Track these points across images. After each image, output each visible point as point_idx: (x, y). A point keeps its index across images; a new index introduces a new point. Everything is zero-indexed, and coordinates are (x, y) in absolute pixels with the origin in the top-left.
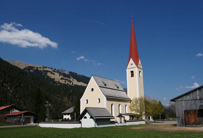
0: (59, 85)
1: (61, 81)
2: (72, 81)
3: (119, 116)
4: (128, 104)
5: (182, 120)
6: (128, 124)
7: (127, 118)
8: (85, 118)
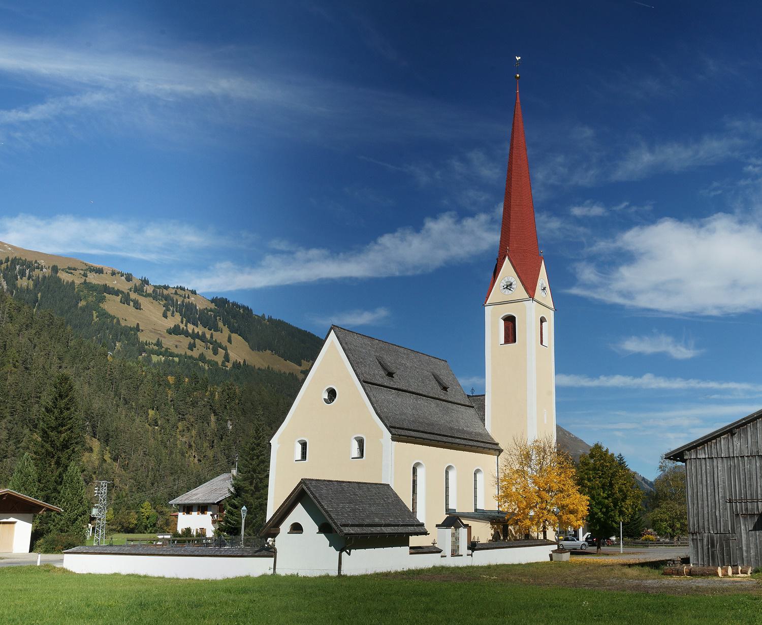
0: (159, 363)
1: (169, 342)
2: (225, 343)
3: (447, 524)
4: (487, 462)
5: (713, 546)
6: (482, 558)
7: (483, 532)
8: (297, 528)
